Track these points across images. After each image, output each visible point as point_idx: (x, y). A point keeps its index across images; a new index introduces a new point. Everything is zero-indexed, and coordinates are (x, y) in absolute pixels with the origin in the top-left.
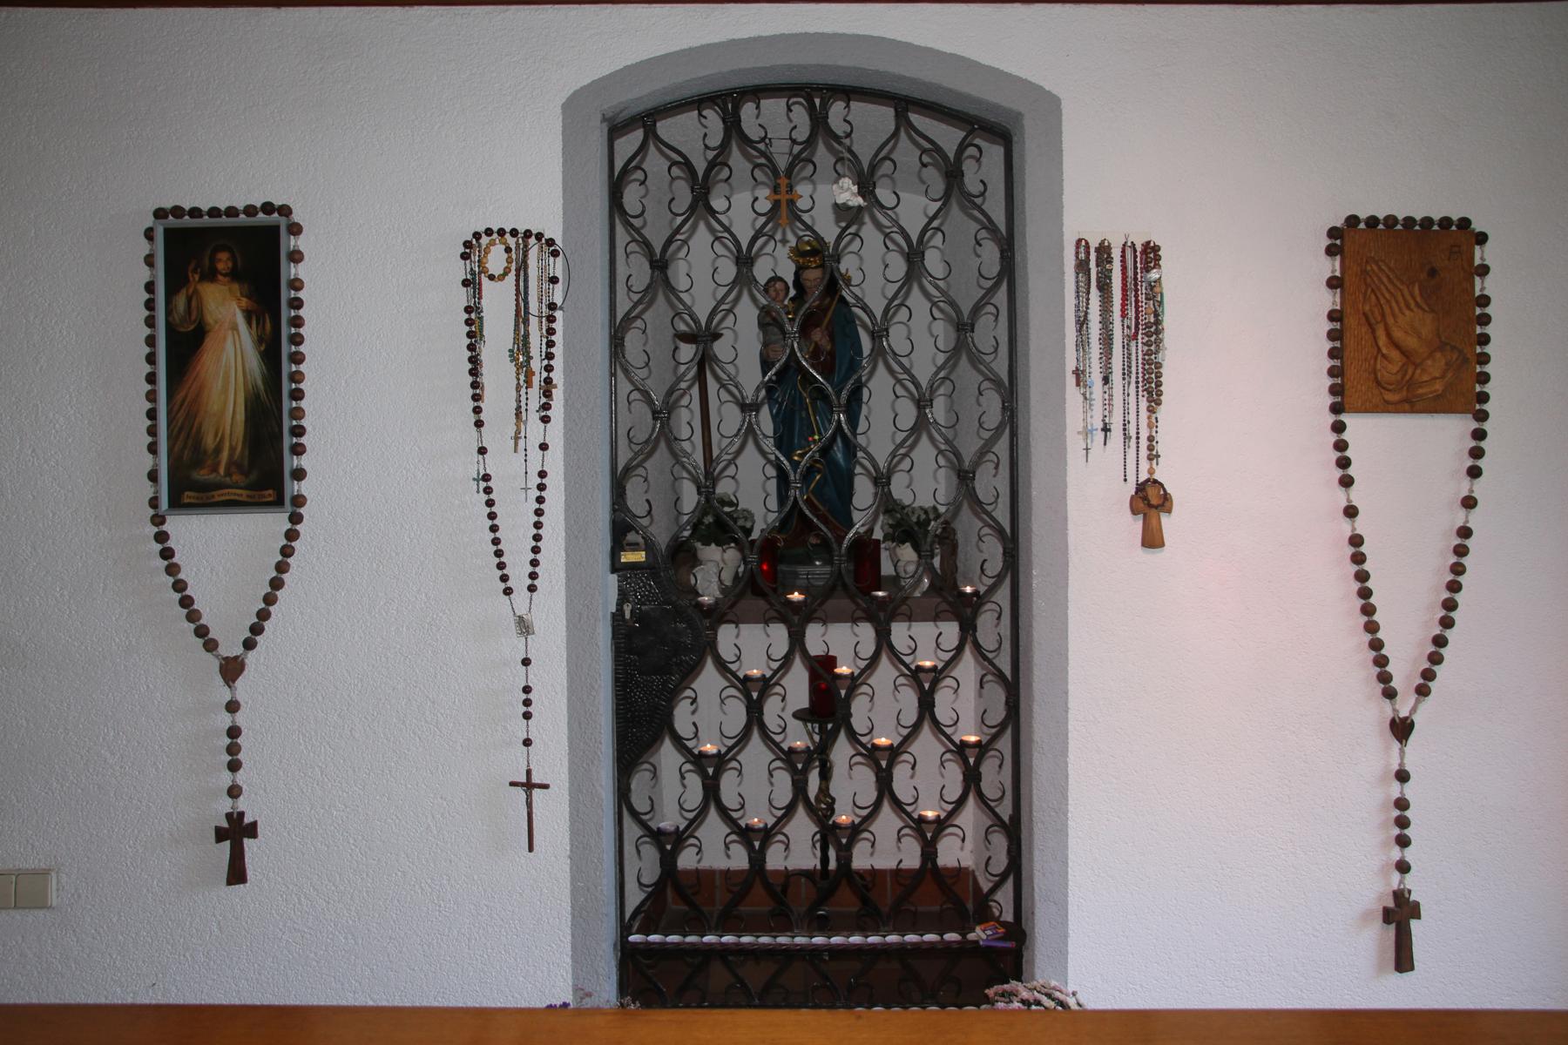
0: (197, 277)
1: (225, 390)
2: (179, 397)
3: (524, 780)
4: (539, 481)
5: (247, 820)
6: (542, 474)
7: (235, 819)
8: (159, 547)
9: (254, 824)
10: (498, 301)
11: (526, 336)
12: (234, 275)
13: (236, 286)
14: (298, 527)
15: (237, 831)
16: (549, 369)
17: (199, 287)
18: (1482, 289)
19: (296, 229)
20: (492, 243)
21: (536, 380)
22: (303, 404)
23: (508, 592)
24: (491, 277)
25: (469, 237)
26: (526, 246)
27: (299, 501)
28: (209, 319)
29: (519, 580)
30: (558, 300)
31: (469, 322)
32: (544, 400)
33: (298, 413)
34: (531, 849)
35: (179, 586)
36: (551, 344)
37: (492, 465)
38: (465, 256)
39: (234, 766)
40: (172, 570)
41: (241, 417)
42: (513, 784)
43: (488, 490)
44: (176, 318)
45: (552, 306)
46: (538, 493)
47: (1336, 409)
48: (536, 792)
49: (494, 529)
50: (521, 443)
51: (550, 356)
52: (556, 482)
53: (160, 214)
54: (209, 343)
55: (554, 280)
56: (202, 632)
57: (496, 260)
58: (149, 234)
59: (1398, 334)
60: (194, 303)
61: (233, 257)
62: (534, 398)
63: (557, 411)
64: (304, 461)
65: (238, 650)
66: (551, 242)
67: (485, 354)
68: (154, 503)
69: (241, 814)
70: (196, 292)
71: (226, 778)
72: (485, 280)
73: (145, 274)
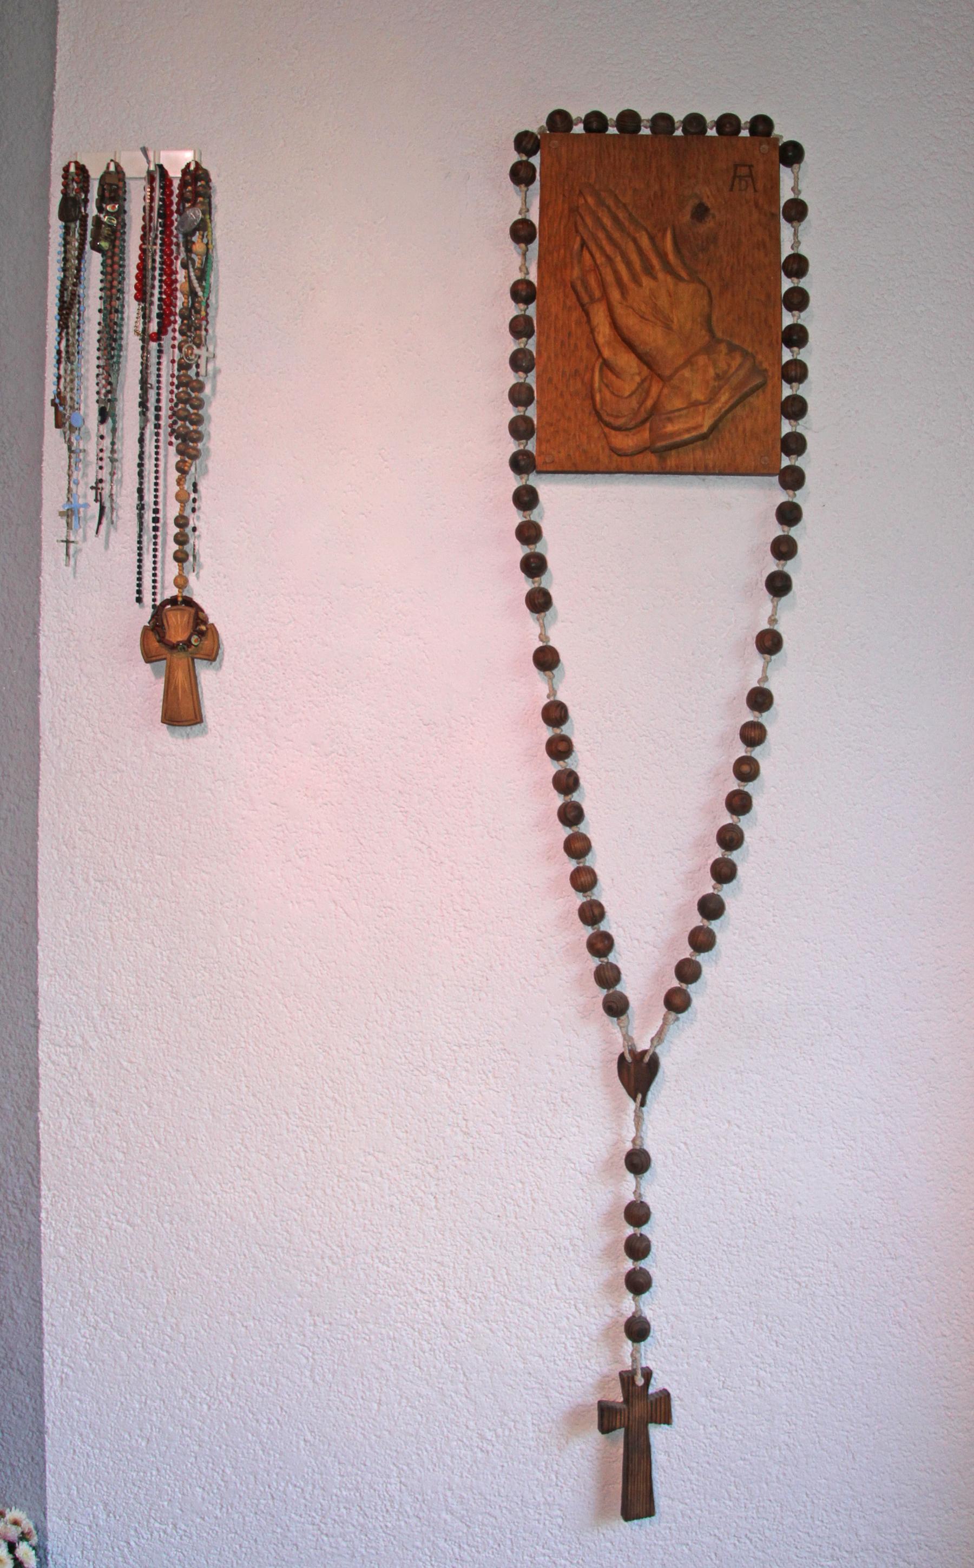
18: (796, 243)
47: (520, 464)
59: (629, 321)
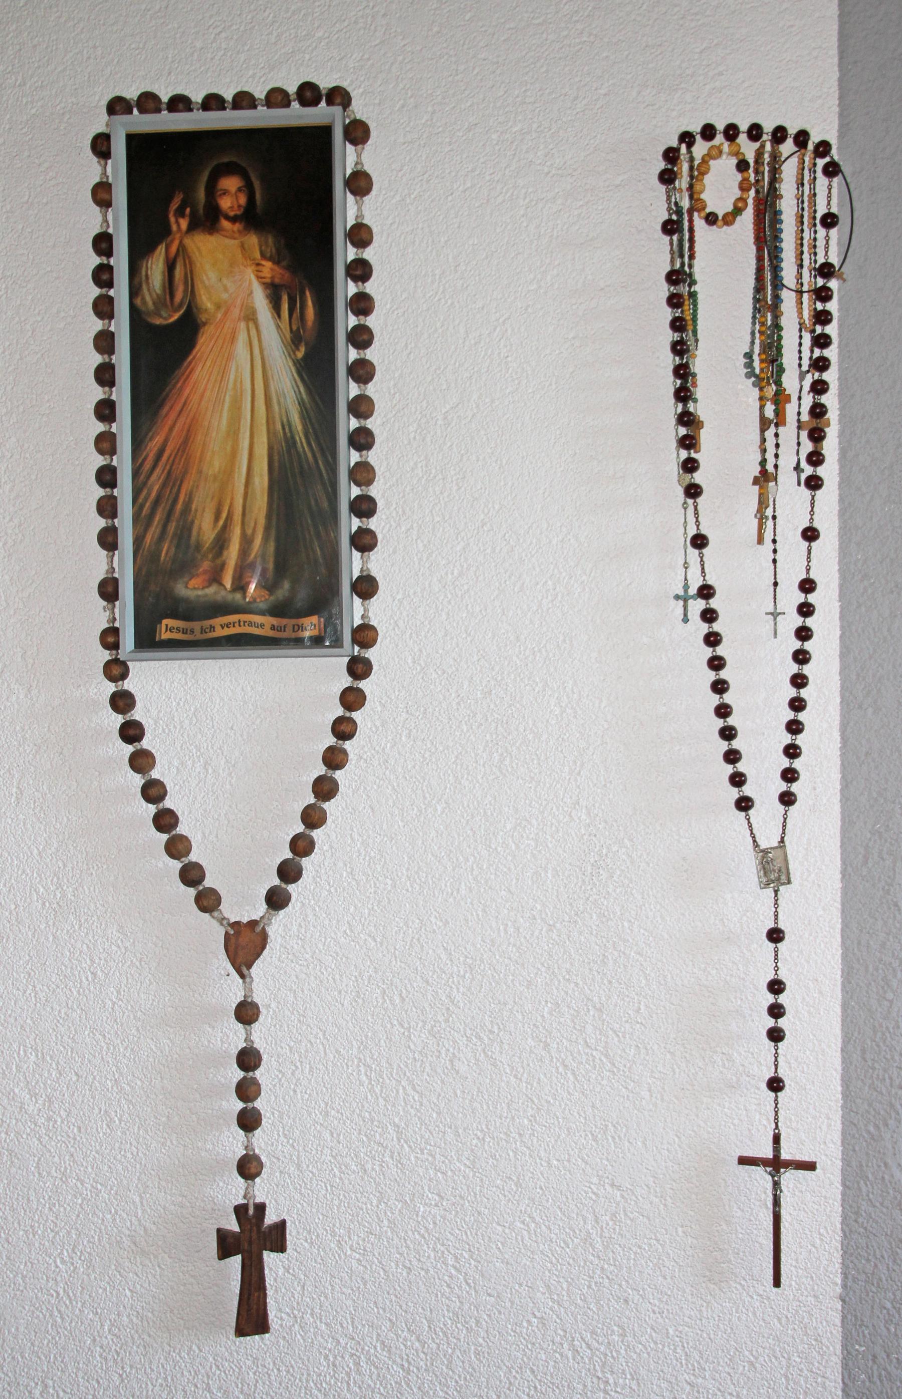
0: (184, 224)
1: (233, 432)
2: (153, 446)
3: (767, 1152)
4: (801, 598)
5: (270, 1218)
6: (807, 586)
7: (250, 1214)
8: (119, 719)
9: (281, 1227)
10: (724, 261)
12: (250, 218)
13: (253, 240)
14: (363, 685)
15: (252, 1238)
17: (188, 242)
19: (358, 133)
20: (715, 154)
22: (373, 457)
23: (744, 804)
24: (711, 219)
27: (365, 635)
28: (206, 301)
29: (764, 785)
33: (363, 474)
34: (777, 1283)
35: (153, 792)
39: (248, 1121)
40: (141, 761)
41: (261, 481)
42: (744, 1161)
43: (709, 616)
44: (148, 300)
46: (799, 621)
48: (788, 1177)
49: (719, 687)
50: (769, 512)
52: (825, 599)
53: (117, 106)
54: (205, 343)
56: (191, 875)
57: (721, 186)
58: (101, 146)
60: (179, 272)
61: (249, 188)
62: (791, 444)
64: (377, 563)
65: (259, 909)
67: (701, 363)
68: (110, 638)
69: (261, 1208)
70: (182, 248)
71: (234, 1143)
72: (699, 223)
73: (92, 220)
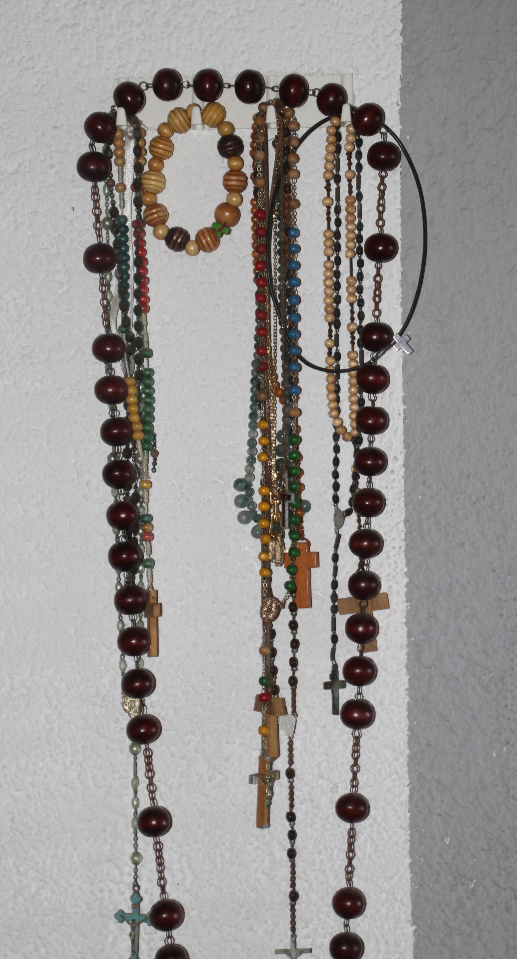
11: (292, 435)
16: (367, 544)
20: (180, 122)
21: (320, 579)
24: (177, 240)
25: (105, 104)
26: (286, 129)
30: (392, 317)
31: (109, 390)
32: (348, 649)
36: (371, 462)
37: (187, 866)
38: (94, 168)
42: (277, 952)
45: (376, 337)
51: (368, 503)
55: (381, 248)
57: (193, 180)
62: (318, 641)
63: (388, 694)
66: (369, 118)
67: (163, 496)
